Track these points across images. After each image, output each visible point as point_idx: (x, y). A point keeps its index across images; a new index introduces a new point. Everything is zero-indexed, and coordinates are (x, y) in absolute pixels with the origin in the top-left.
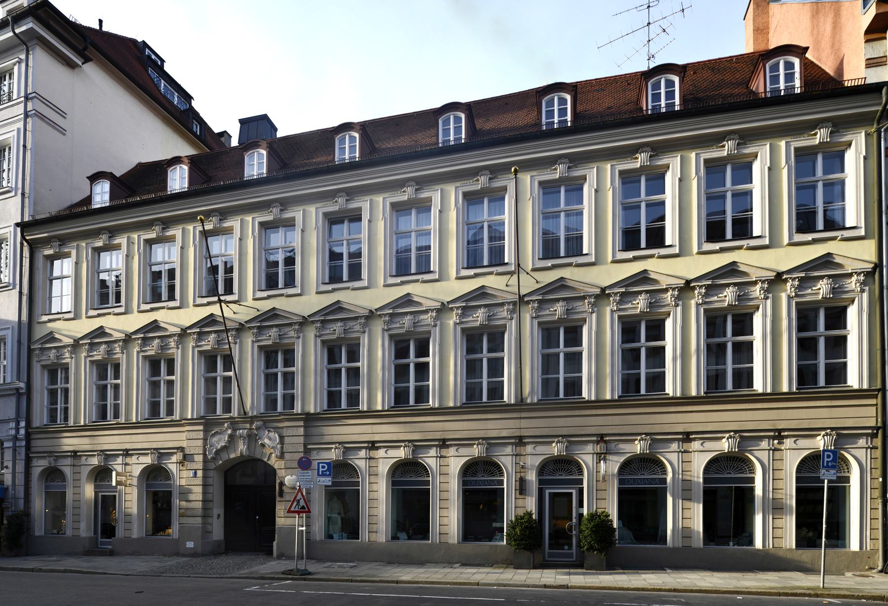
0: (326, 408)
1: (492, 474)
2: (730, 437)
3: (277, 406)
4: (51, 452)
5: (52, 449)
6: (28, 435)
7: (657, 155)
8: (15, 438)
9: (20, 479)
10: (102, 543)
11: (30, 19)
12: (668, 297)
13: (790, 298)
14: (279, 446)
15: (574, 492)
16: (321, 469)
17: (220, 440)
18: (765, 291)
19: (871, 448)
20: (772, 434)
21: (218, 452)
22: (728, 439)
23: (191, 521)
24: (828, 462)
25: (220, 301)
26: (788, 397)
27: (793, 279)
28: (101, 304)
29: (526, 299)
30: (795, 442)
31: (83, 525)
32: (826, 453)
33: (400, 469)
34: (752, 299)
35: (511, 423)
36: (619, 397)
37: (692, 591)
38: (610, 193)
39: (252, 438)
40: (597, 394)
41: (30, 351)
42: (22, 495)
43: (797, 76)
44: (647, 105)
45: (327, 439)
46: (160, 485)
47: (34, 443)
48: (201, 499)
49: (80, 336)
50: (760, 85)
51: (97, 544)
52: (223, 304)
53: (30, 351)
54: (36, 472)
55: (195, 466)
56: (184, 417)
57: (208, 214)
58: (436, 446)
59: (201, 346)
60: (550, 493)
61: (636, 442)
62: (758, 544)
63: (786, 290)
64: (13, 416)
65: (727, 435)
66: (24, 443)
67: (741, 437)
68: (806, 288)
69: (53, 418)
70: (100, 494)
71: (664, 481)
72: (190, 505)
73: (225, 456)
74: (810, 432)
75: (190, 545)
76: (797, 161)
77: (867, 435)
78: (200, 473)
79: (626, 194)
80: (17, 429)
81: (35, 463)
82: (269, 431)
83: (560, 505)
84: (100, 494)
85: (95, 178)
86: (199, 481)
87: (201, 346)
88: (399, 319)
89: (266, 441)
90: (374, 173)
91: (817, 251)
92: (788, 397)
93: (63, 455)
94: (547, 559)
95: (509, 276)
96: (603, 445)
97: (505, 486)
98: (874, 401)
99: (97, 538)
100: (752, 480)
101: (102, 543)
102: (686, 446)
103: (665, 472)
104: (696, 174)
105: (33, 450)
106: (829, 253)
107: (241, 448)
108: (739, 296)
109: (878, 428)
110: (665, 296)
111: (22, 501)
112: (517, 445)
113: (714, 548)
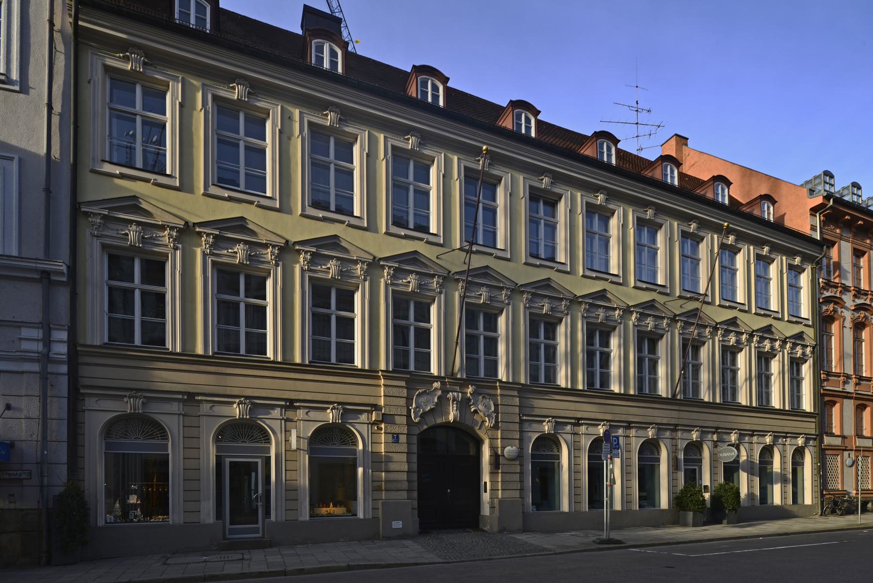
0: (106, 340)
1: (252, 439)
2: (549, 421)
3: (478, 372)
4: (138, 390)
5: (144, 385)
7: (345, 121)
8: (45, 358)
9: (60, 430)
10: (232, 532)
12: (358, 269)
13: (303, 271)
14: (494, 415)
15: (259, 461)
17: (428, 402)
18: (175, 240)
19: (184, 415)
20: (283, 403)
21: (423, 416)
22: (239, 404)
23: (394, 495)
26: (300, 368)
27: (306, 252)
28: (246, 188)
29: (382, 263)
30: (307, 413)
33: (323, 435)
34: (263, 262)
35: (675, 414)
36: (214, 353)
37: (746, 537)
38: (458, 183)
39: (464, 404)
42: (62, 455)
44: (413, 91)
45: (537, 412)
46: (334, 450)
47: (85, 371)
48: (406, 468)
49: (578, 295)
50: (648, 174)
55: (396, 429)
56: (517, 381)
57: (542, 172)
58: (281, 406)
59: (397, 285)
61: (329, 411)
62: (565, 507)
63: (299, 262)
64: (37, 316)
65: (237, 401)
66: (64, 369)
67: (344, 409)
68: (399, 279)
69: (120, 330)
70: (228, 460)
71: (354, 452)
72: (393, 476)
73: (432, 421)
74: (320, 405)
75: (397, 525)
76: (394, 161)
77: (281, 406)
78: (403, 438)
79: (314, 149)
80: (47, 341)
81: (90, 403)
82: (484, 397)
86: (404, 448)
87: (397, 285)
88: (120, 227)
89: (481, 407)
90: (584, 170)
91: (407, 247)
92: (300, 368)
93: (166, 397)
94: (228, 536)
95: (686, 301)
97: (170, 451)
98: (813, 420)
100: (558, 457)
101: (232, 532)
102: (290, 414)
103: (355, 443)
104: (203, 105)
106: (242, 217)
107: (452, 415)
108: (250, 255)
109: (817, 435)
110: (264, 252)
111: (64, 469)
112: (574, 425)
113: (594, 511)
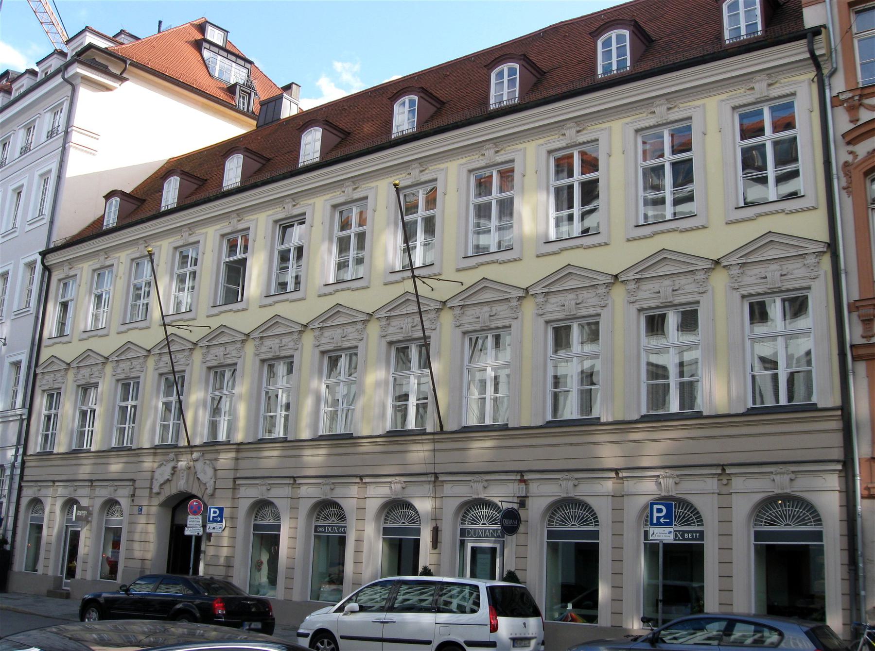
6: (23, 462)
11: (76, 64)
16: (655, 515)
24: (658, 518)
25: (414, 277)
31: (297, 585)
32: (655, 507)
40: (228, 436)
41: (35, 375)
43: (758, 12)
51: (61, 586)
52: (416, 279)
53: (35, 375)
54: (24, 502)
60: (472, 548)
83: (182, 551)
84: (70, 529)
85: (108, 197)
96: (523, 485)
99: (62, 578)
105: (25, 478)
